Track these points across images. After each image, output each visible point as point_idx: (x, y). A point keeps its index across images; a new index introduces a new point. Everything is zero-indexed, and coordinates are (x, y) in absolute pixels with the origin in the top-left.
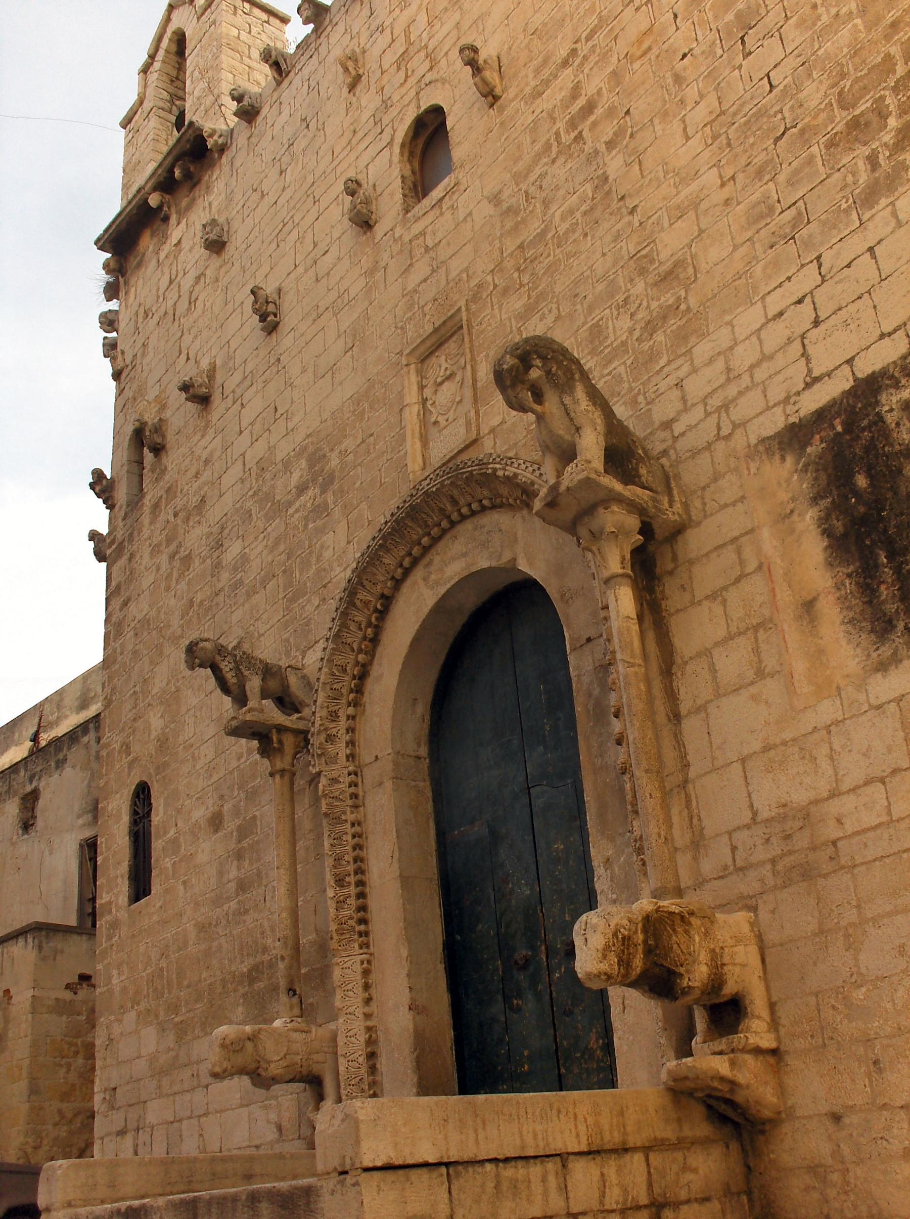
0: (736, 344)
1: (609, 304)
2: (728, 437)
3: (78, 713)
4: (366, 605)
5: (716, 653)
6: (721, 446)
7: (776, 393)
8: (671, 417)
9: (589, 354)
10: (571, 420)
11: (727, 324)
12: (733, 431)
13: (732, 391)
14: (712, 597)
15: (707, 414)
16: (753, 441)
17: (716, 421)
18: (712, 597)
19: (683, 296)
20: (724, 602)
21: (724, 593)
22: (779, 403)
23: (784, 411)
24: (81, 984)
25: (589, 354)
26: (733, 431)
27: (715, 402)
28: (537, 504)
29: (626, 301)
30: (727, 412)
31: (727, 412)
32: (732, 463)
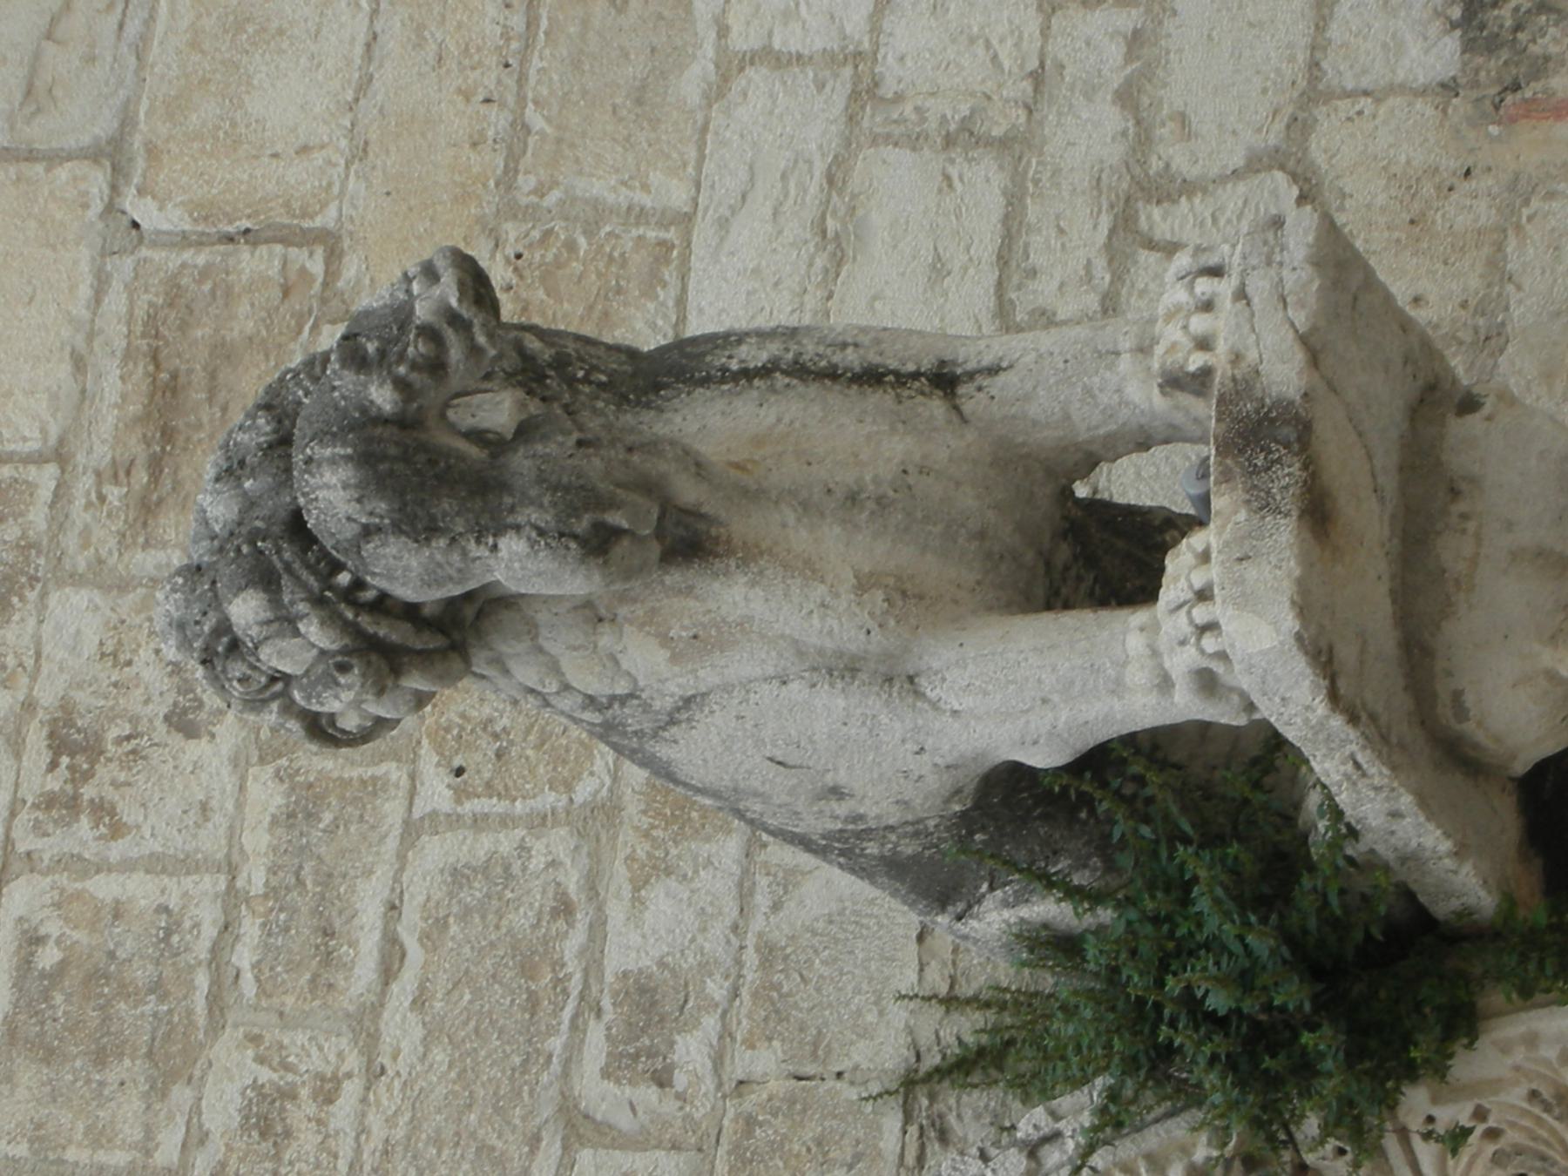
9: (159, 1089)
10: (871, 377)
11: (717, 91)
13: (1087, 136)
16: (1440, 55)
25: (159, 1089)
29: (72, 743)
31: (1169, 189)
32: (1471, 210)
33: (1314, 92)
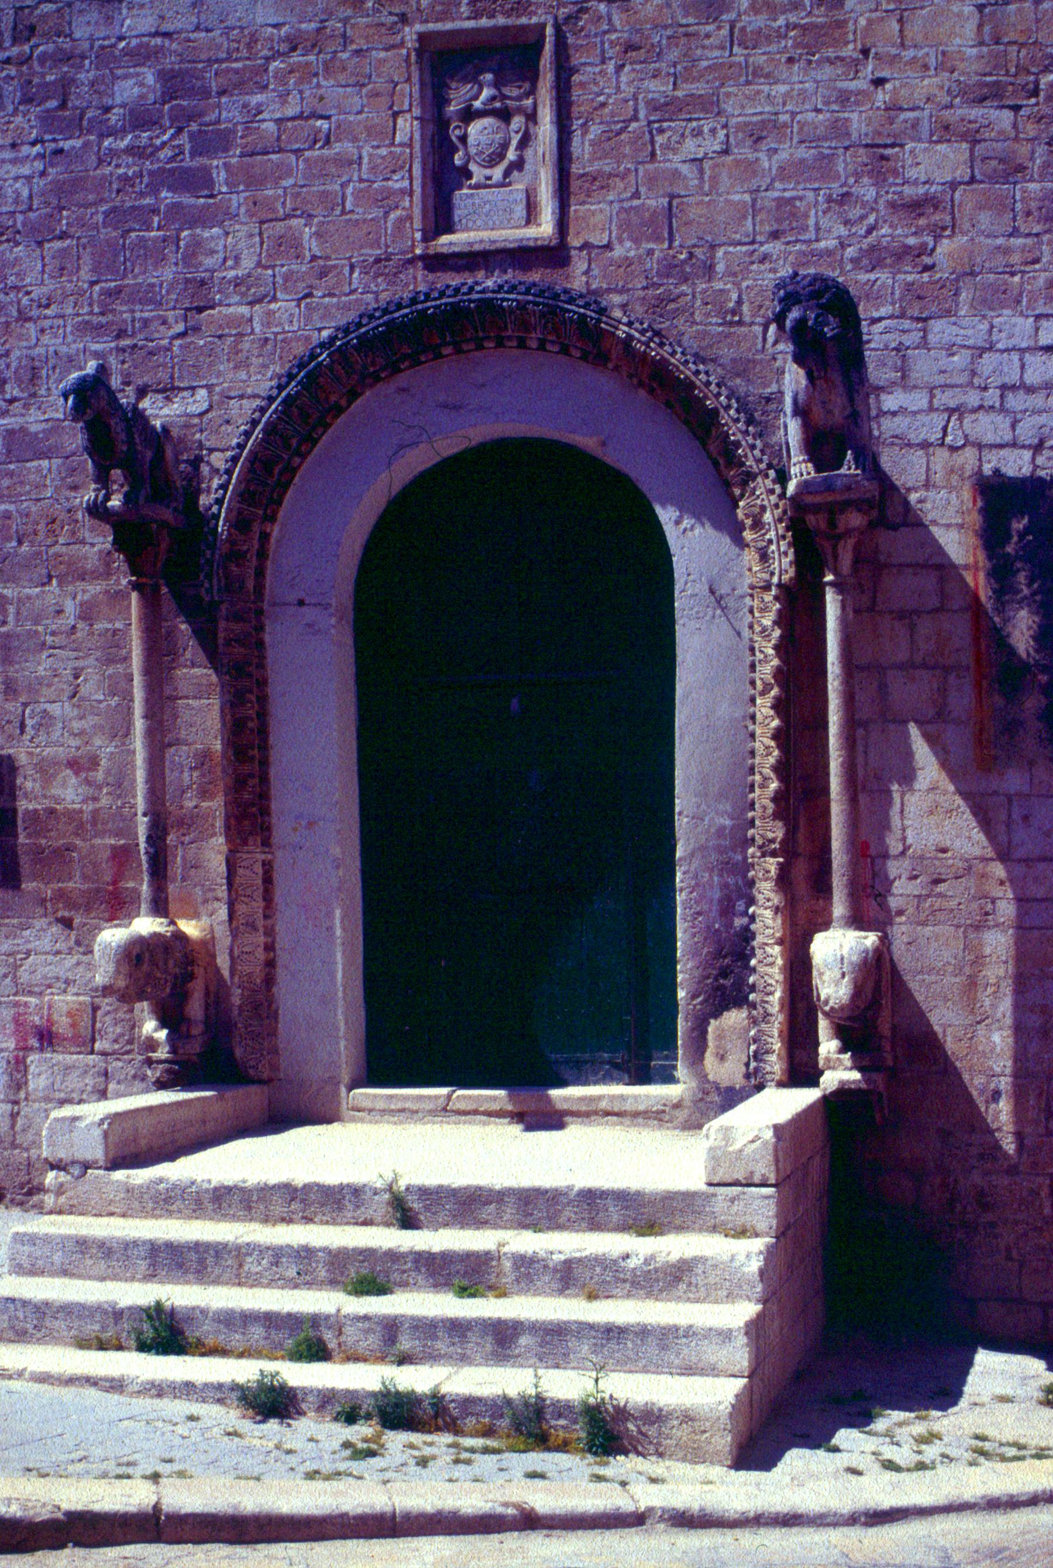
0: (990, 349)
1: (816, 185)
2: (953, 449)
3: (703, 1260)
4: (318, 397)
5: (890, 673)
6: (942, 454)
7: (1026, 431)
8: (881, 384)
12: (964, 445)
14: (902, 615)
15: (931, 409)
17: (944, 423)
18: (902, 615)
19: (931, 246)
20: (912, 629)
21: (915, 617)
22: (1030, 447)
23: (1033, 459)
24: (753, 1006)
26: (964, 445)
27: (944, 399)
28: (269, 856)
30: (960, 419)
31: (960, 419)
33: (980, 446)
